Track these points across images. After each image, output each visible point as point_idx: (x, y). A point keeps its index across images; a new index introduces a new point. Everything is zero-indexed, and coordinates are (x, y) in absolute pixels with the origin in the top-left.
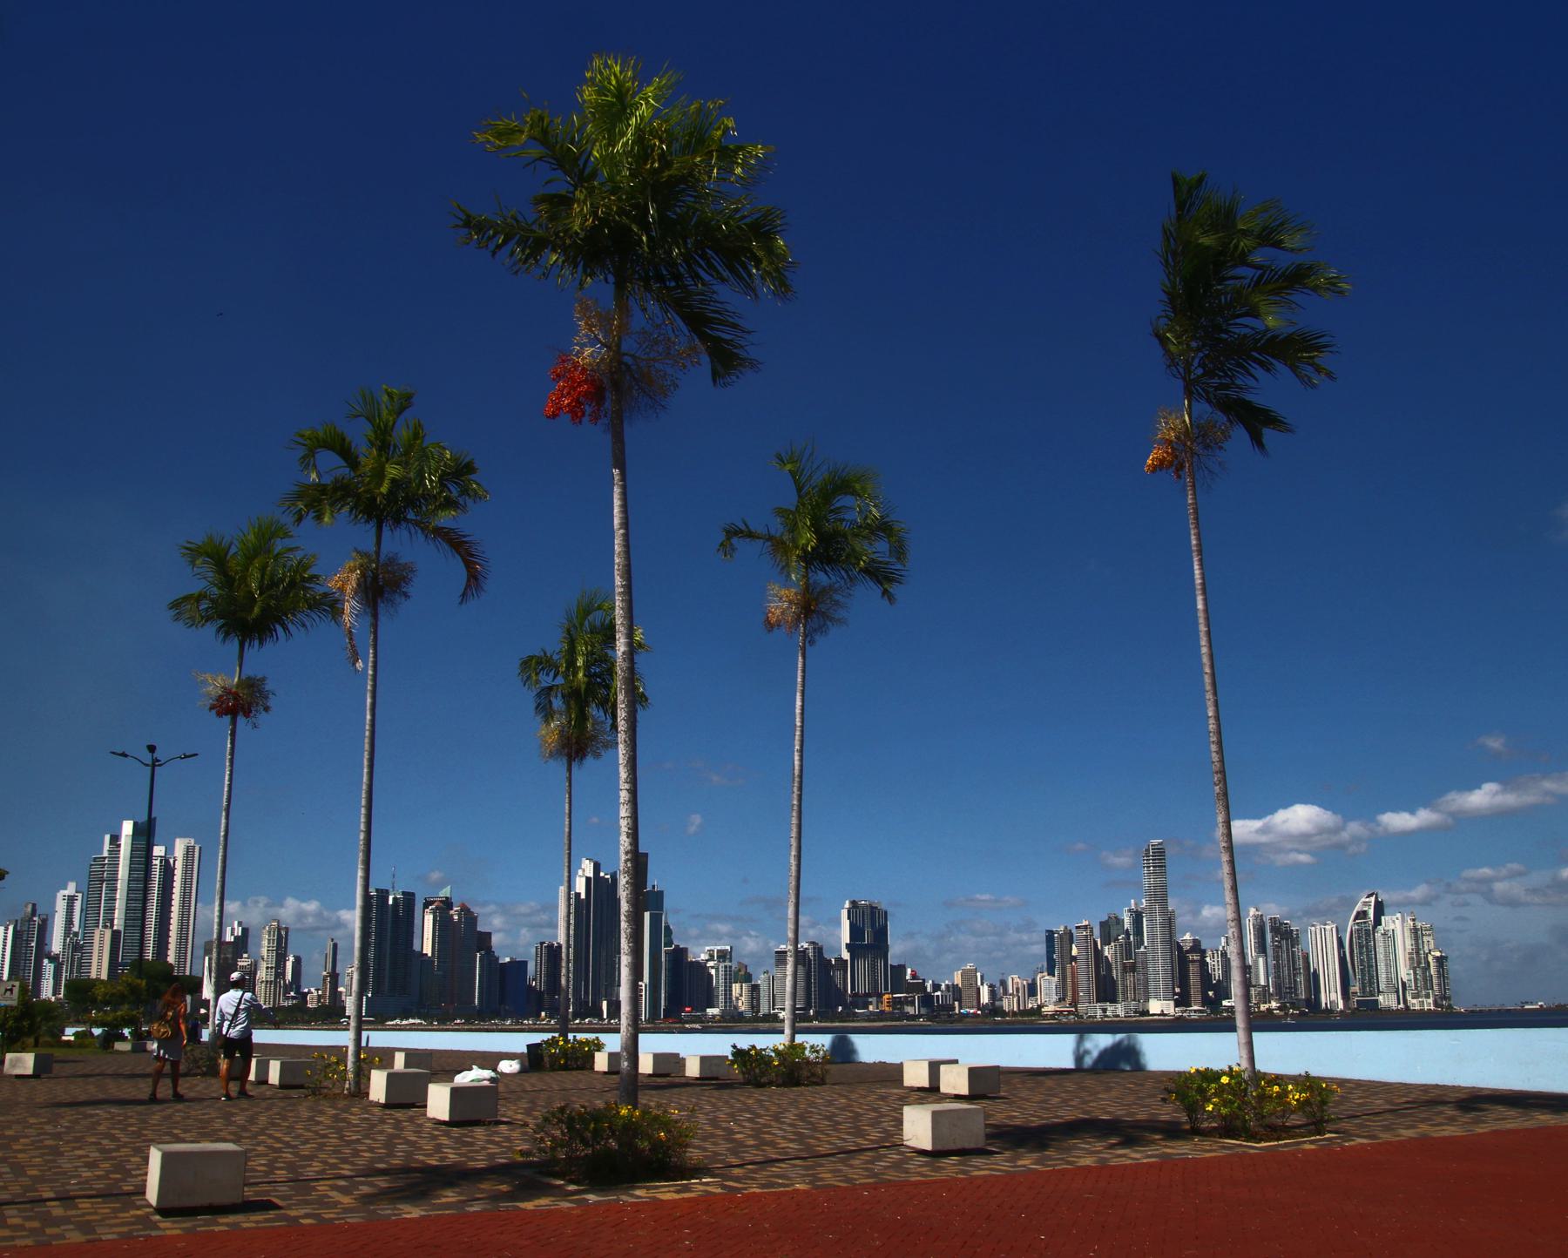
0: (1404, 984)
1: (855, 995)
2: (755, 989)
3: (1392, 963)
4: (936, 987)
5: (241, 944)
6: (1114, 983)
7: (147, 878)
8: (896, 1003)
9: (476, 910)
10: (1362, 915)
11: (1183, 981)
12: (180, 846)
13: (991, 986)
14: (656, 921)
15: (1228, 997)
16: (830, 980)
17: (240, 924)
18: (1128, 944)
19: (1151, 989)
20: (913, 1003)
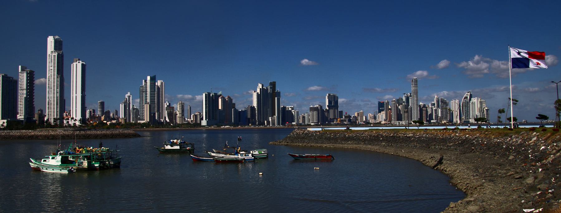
3: (474, 110)
6: (401, 115)
9: (232, 98)
10: (466, 98)
15: (433, 119)
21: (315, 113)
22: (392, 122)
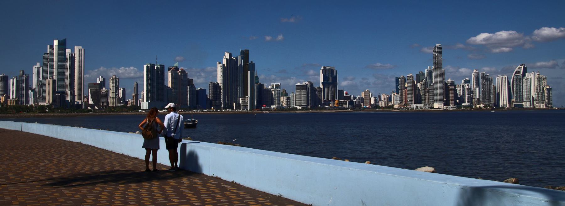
0: (533, 98)
1: (325, 101)
2: (289, 98)
4: (355, 98)
5: (103, 84)
6: (421, 96)
7: (65, 60)
8: (340, 103)
10: (518, 72)
11: (447, 96)
12: (77, 49)
13: (375, 98)
14: (252, 74)
15: (464, 102)
16: (316, 95)
17: (102, 77)
18: (427, 82)
19: (435, 99)
20: (346, 104)
21: (303, 92)
22: (408, 105)
